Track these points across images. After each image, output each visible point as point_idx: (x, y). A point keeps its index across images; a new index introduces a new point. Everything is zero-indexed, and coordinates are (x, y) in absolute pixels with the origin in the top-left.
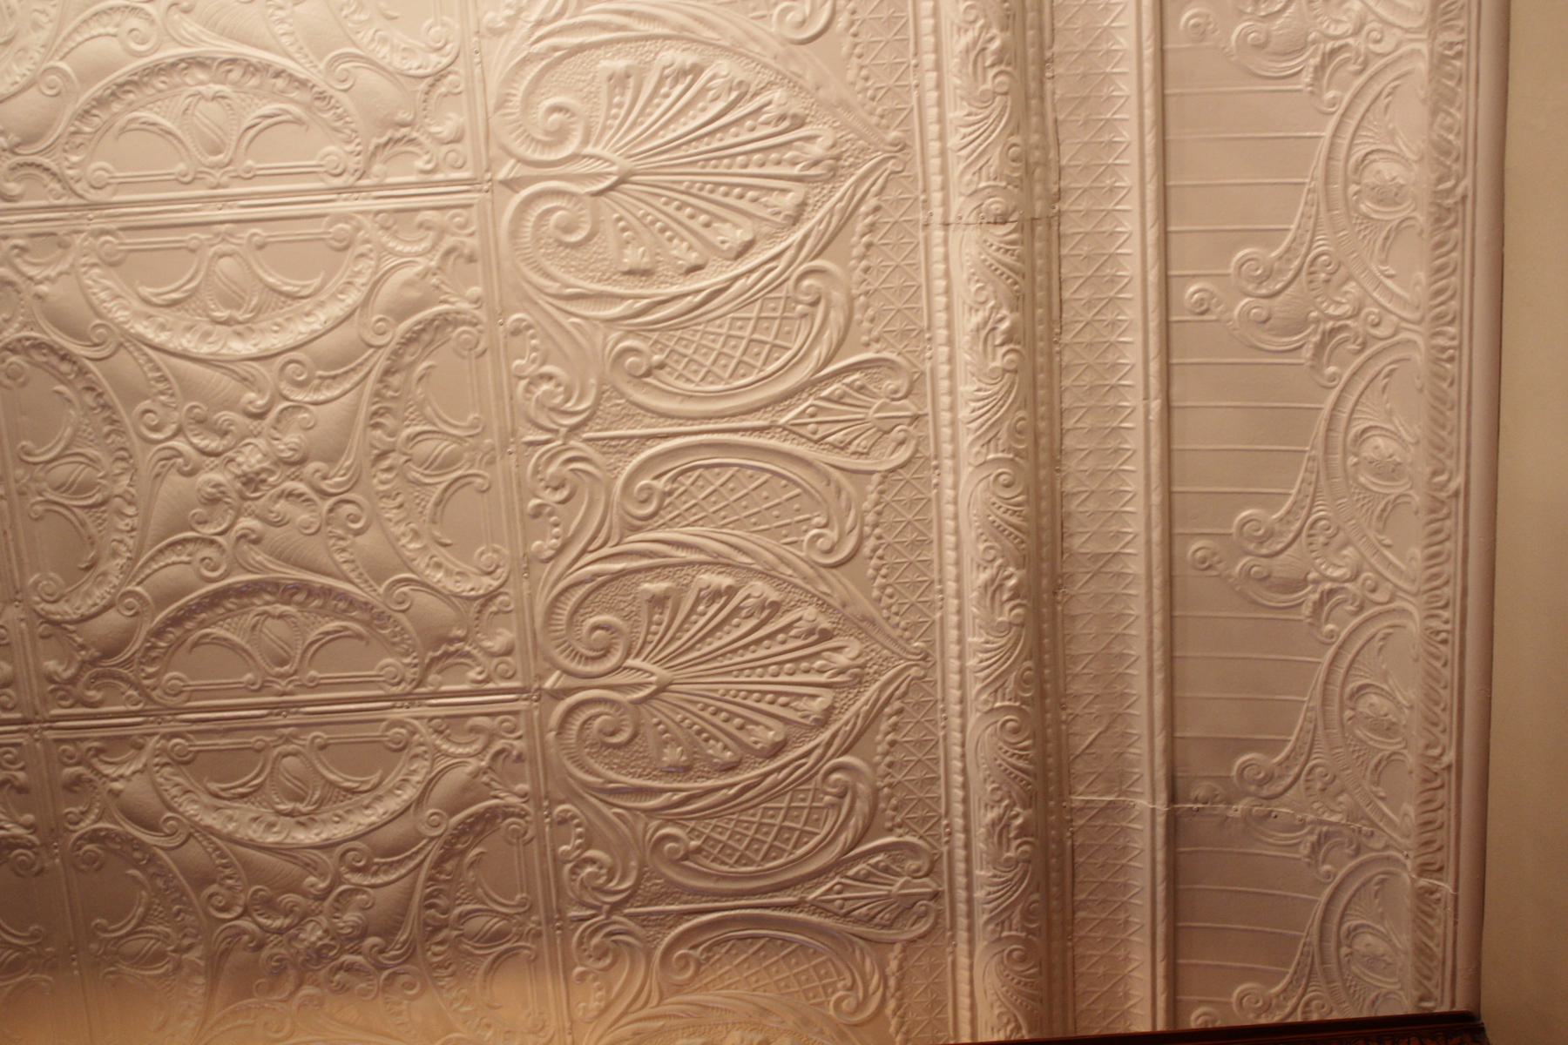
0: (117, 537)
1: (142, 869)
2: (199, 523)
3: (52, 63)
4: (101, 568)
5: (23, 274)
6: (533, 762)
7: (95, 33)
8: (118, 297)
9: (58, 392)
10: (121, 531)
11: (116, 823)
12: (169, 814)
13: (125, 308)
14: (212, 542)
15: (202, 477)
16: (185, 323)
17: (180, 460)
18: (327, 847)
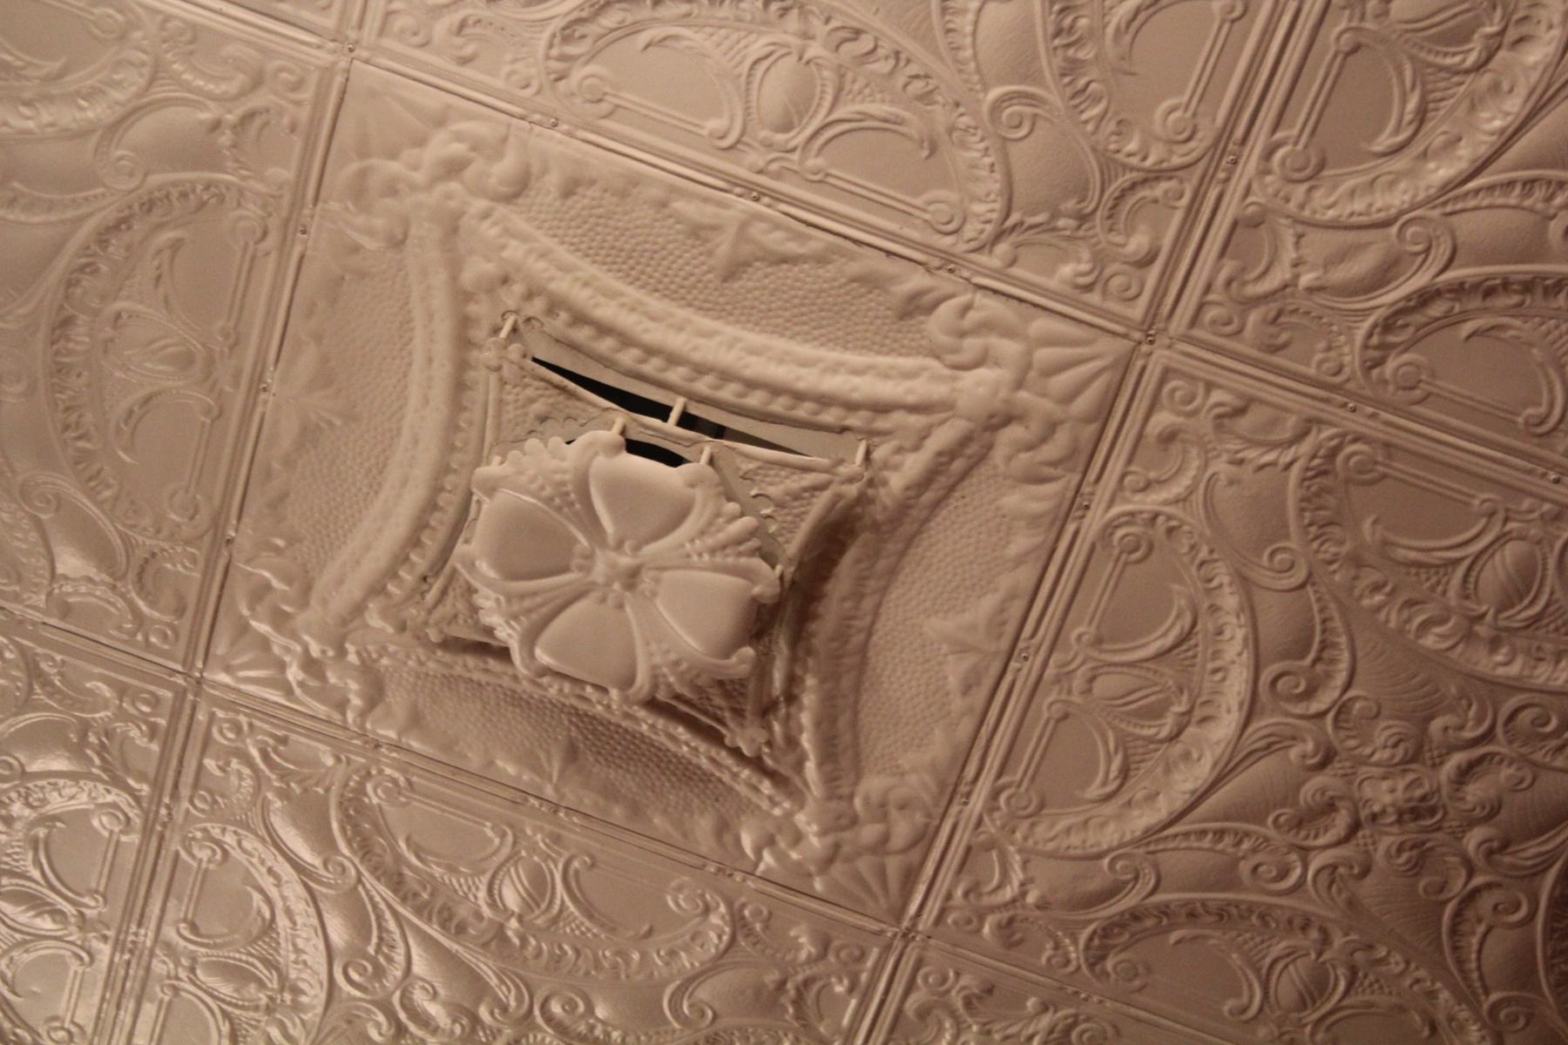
0: (1408, 982)
1: (1172, 927)
2: (1441, 890)
3: (1486, 1007)
4: (1441, 1017)
5: (1006, 905)
6: (673, 189)
7: (1475, 947)
8: (1086, 823)
9: (1178, 942)
10: (1402, 974)
11: (1090, 922)
12: (1106, 861)
13: (1103, 825)
14: (1477, 891)
15: (1379, 856)
16: (1159, 770)
17: (1341, 870)
18: (1251, 711)
